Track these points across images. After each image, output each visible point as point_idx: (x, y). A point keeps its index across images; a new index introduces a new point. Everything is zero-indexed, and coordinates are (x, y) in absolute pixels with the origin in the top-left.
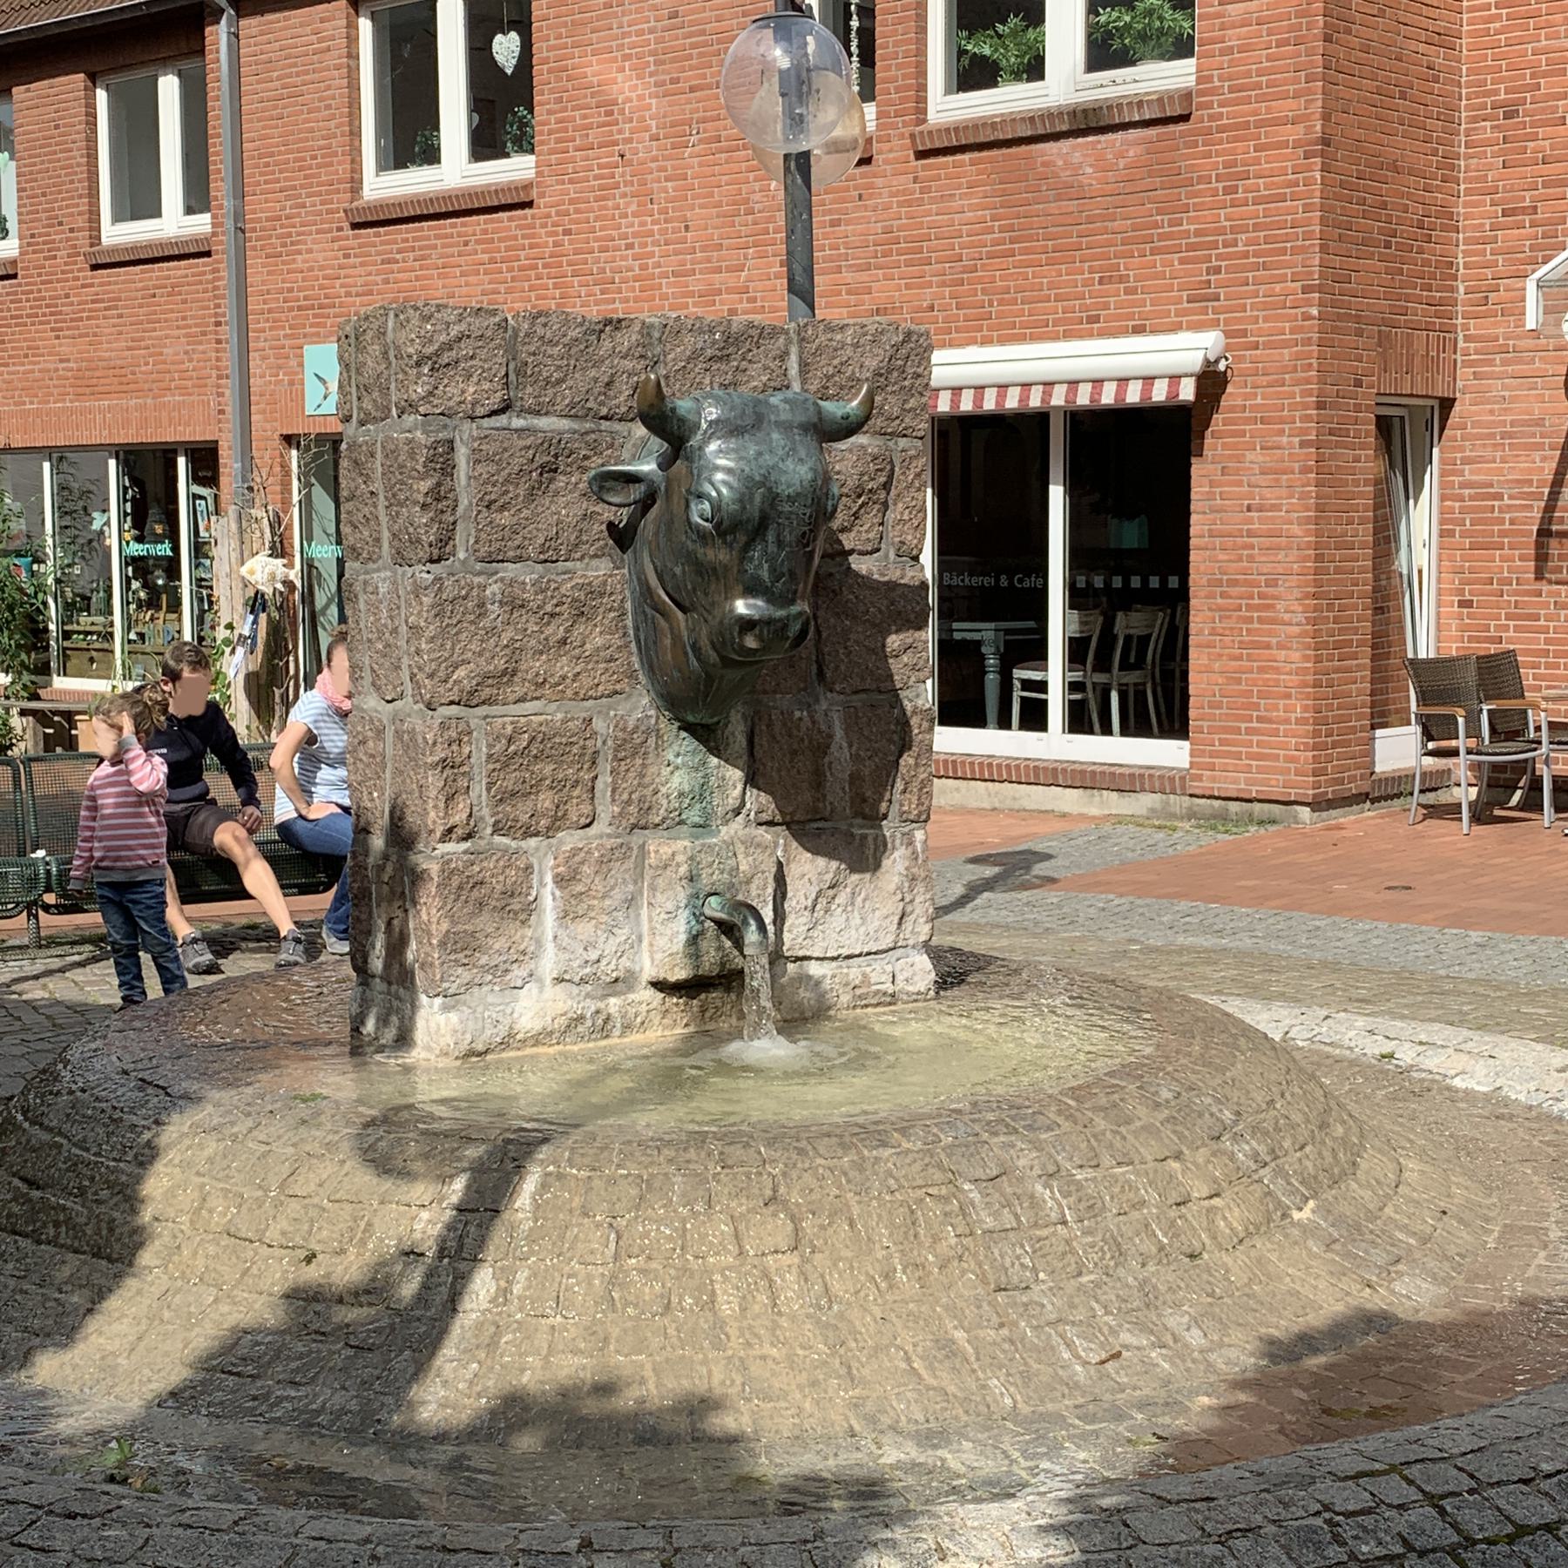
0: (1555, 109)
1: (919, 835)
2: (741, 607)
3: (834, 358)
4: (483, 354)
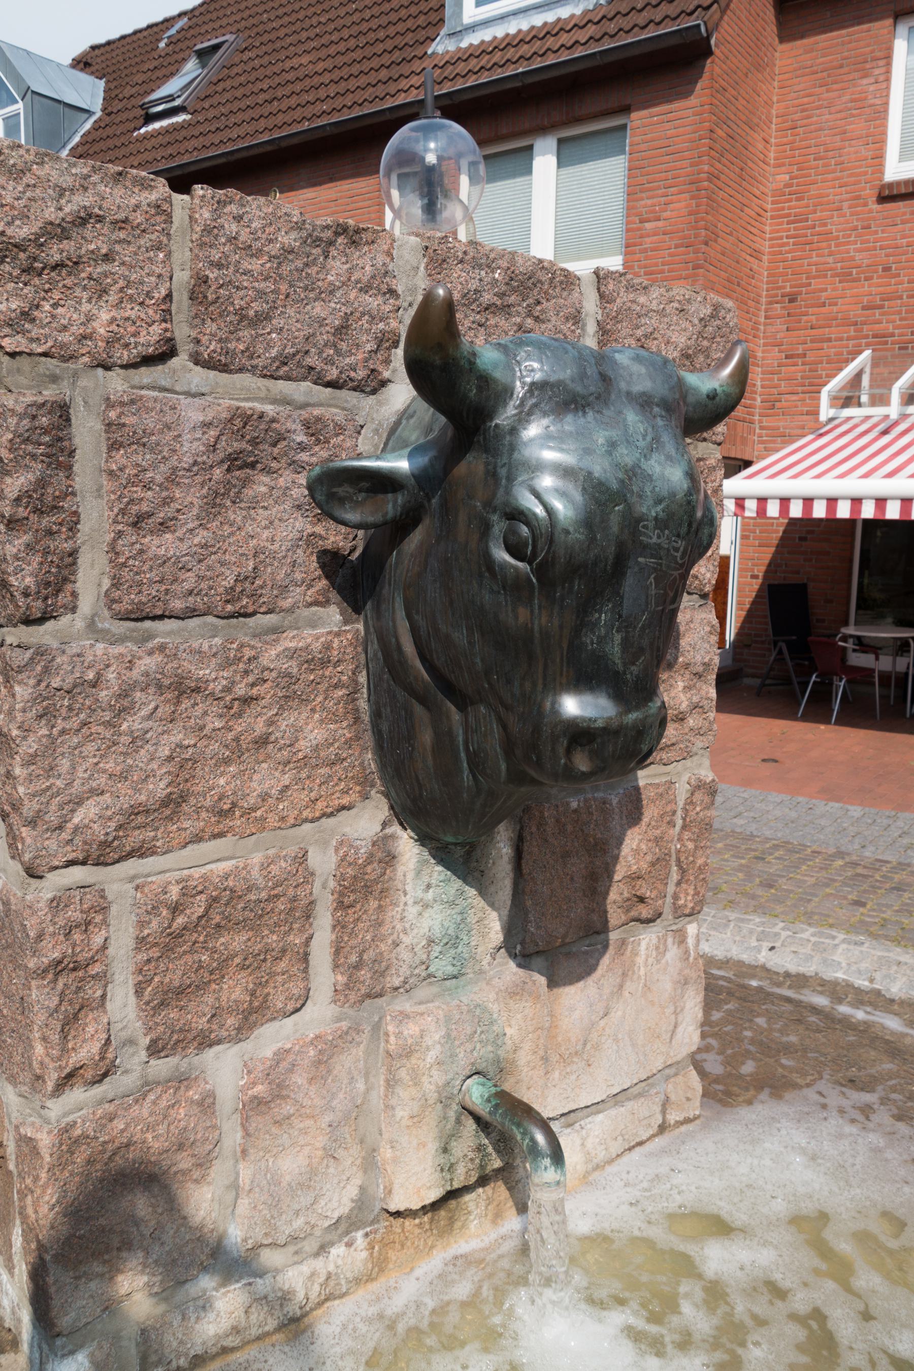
0: (819, 298)
1: (692, 929)
2: (572, 706)
3: (638, 327)
4: (125, 253)
